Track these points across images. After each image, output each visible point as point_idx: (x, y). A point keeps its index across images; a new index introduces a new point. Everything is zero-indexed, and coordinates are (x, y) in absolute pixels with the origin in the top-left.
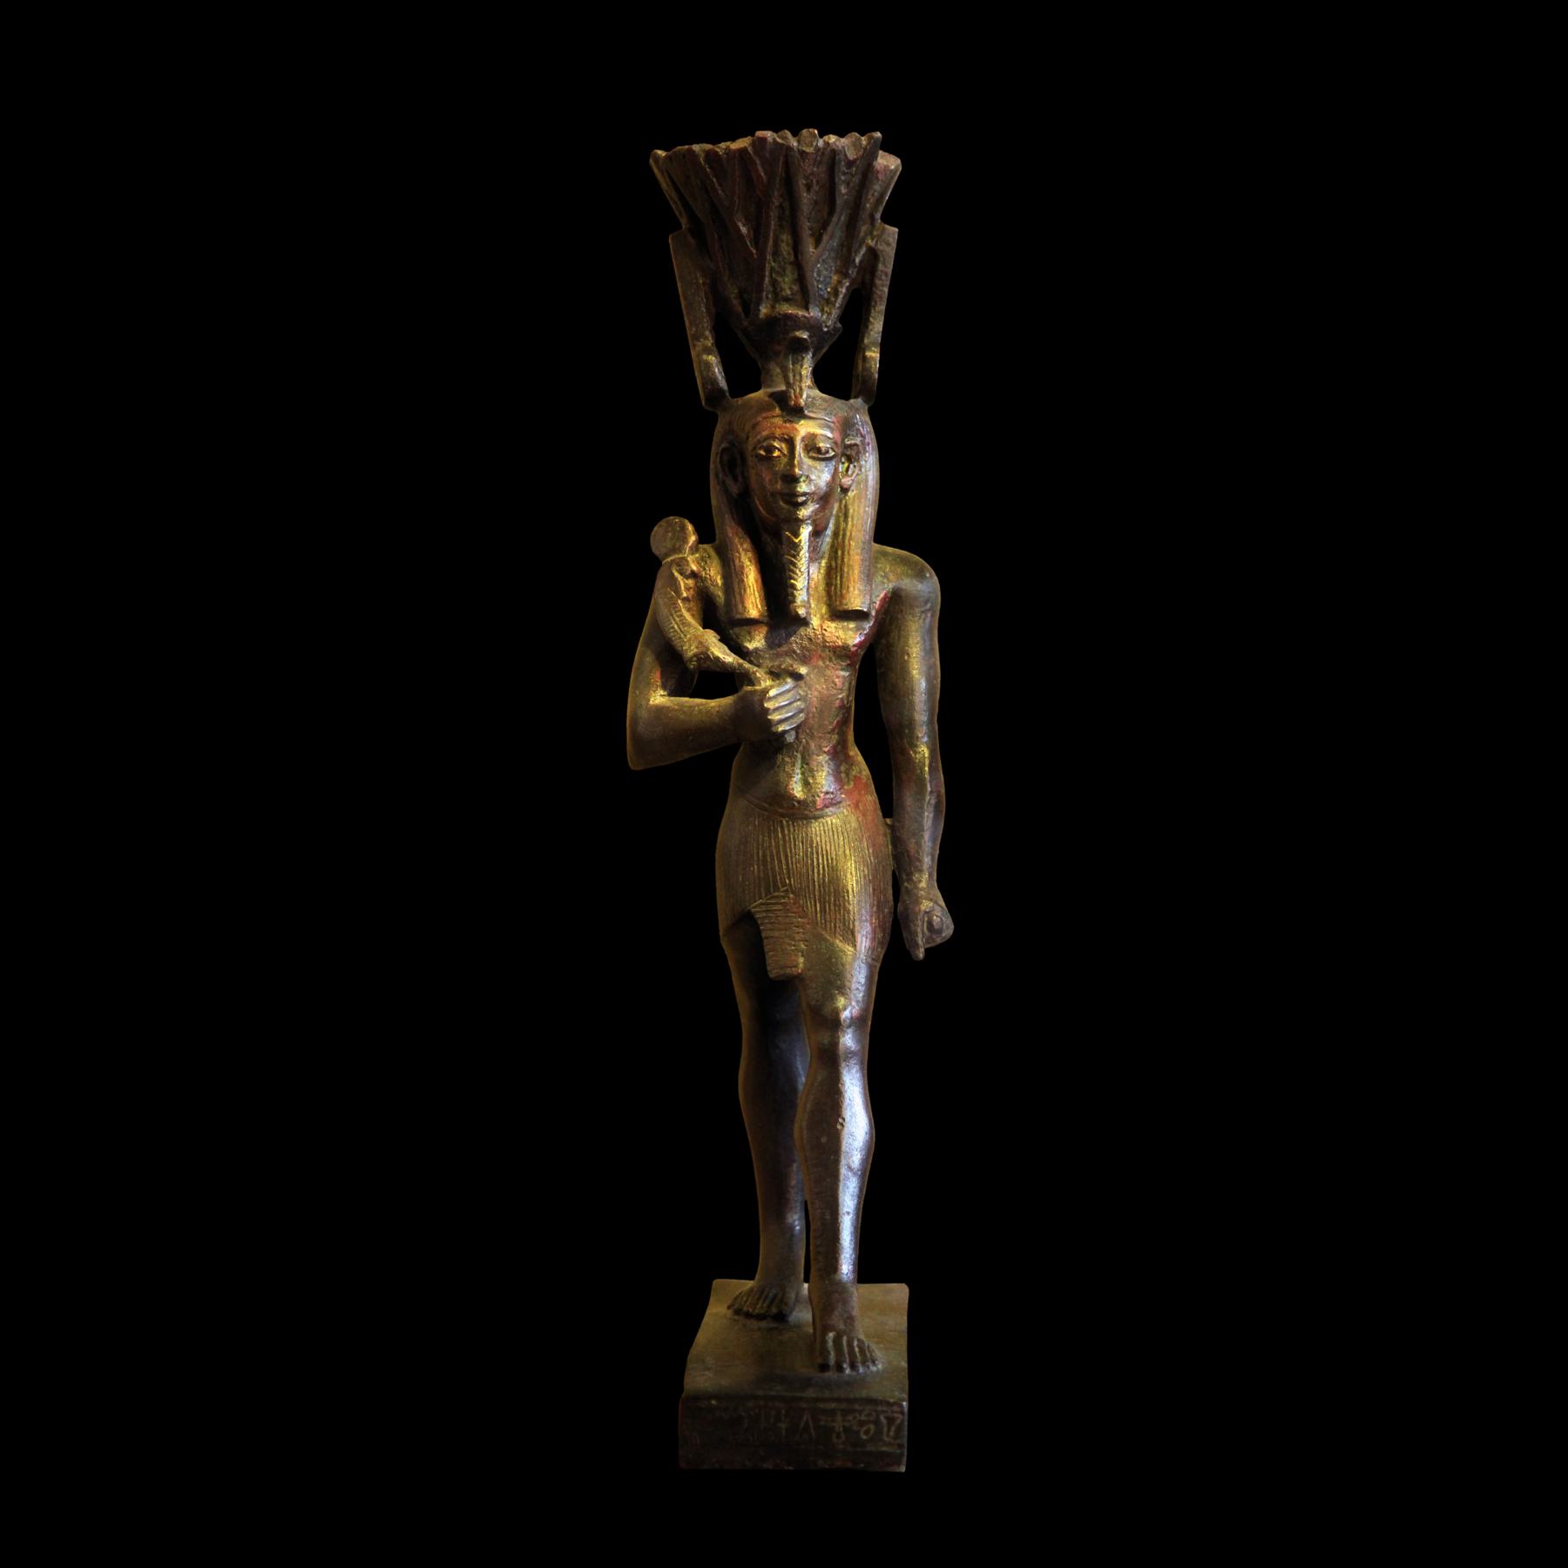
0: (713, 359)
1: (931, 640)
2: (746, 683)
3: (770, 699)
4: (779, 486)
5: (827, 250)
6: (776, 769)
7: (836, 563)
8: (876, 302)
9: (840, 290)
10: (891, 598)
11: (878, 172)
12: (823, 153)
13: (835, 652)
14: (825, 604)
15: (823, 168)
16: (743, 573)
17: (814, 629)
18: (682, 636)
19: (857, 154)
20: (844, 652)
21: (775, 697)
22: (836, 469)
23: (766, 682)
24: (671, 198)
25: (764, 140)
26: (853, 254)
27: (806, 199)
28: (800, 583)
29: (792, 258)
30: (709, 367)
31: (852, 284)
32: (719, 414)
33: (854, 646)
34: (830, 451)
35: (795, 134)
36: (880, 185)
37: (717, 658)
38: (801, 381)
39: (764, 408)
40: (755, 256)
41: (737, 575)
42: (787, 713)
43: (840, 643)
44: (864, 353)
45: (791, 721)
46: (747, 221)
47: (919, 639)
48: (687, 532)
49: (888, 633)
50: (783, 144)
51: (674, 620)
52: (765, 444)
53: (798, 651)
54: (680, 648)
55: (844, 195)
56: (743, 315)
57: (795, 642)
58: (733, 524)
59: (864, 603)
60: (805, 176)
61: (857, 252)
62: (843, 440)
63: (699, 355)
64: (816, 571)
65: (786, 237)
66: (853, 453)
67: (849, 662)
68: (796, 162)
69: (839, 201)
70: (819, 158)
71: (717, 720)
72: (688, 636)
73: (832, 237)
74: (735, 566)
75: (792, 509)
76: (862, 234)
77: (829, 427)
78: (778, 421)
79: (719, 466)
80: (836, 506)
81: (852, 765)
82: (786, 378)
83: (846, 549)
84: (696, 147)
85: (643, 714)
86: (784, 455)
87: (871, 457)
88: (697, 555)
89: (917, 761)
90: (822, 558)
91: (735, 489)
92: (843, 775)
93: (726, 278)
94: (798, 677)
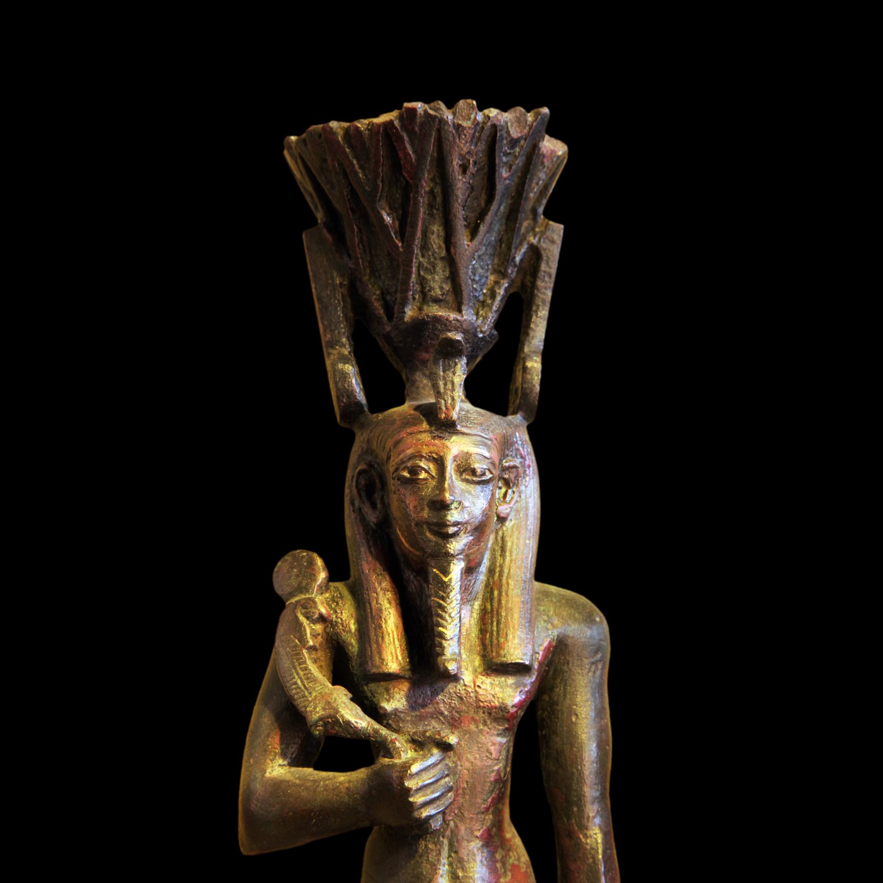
0: (350, 369)
1: (602, 695)
2: (382, 753)
3: (412, 776)
4: (426, 513)
5: (485, 245)
6: (418, 859)
7: (492, 605)
8: (538, 306)
9: (498, 291)
10: (556, 647)
11: (544, 156)
12: (483, 128)
13: (490, 714)
14: (479, 654)
15: (482, 146)
16: (380, 617)
17: (465, 685)
18: (307, 694)
19: (521, 132)
20: (501, 713)
21: (418, 773)
22: (493, 495)
23: (406, 753)
24: (306, 190)
25: (414, 110)
26: (513, 251)
27: (461, 184)
28: (450, 630)
29: (443, 253)
30: (346, 377)
31: (510, 286)
32: (356, 431)
33: (513, 706)
34: (487, 473)
35: (450, 106)
36: (545, 173)
37: (348, 723)
38: (453, 390)
39: (409, 422)
40: (401, 249)
41: (373, 617)
42: (433, 793)
43: (497, 703)
44: (524, 363)
45: (438, 802)
46: (392, 210)
47: (589, 696)
48: (316, 567)
49: (552, 689)
50: (436, 117)
51: (298, 674)
52: (409, 464)
53: (446, 713)
54: (303, 709)
55: (505, 179)
56: (385, 319)
57: (444, 701)
58: (370, 559)
59: (525, 654)
60: (460, 155)
61: (517, 248)
62: (501, 461)
63: (334, 365)
64: (468, 614)
65: (436, 228)
66: (512, 476)
67: (507, 726)
68: (451, 139)
69: (500, 187)
70: (477, 134)
71: (346, 799)
72: (314, 694)
73: (489, 230)
74: (371, 608)
75: (440, 541)
76: (523, 230)
77: (485, 445)
78: (426, 437)
79: (354, 489)
80: (492, 538)
81: (509, 850)
82: (435, 387)
83: (504, 588)
84: (334, 124)
85: (258, 787)
86: (433, 477)
87: (532, 481)
88: (327, 595)
89: (588, 847)
90: (475, 599)
91: (372, 518)
92: (499, 865)
93: (366, 278)
94: (446, 747)
